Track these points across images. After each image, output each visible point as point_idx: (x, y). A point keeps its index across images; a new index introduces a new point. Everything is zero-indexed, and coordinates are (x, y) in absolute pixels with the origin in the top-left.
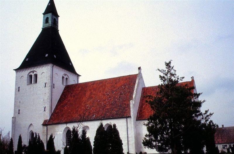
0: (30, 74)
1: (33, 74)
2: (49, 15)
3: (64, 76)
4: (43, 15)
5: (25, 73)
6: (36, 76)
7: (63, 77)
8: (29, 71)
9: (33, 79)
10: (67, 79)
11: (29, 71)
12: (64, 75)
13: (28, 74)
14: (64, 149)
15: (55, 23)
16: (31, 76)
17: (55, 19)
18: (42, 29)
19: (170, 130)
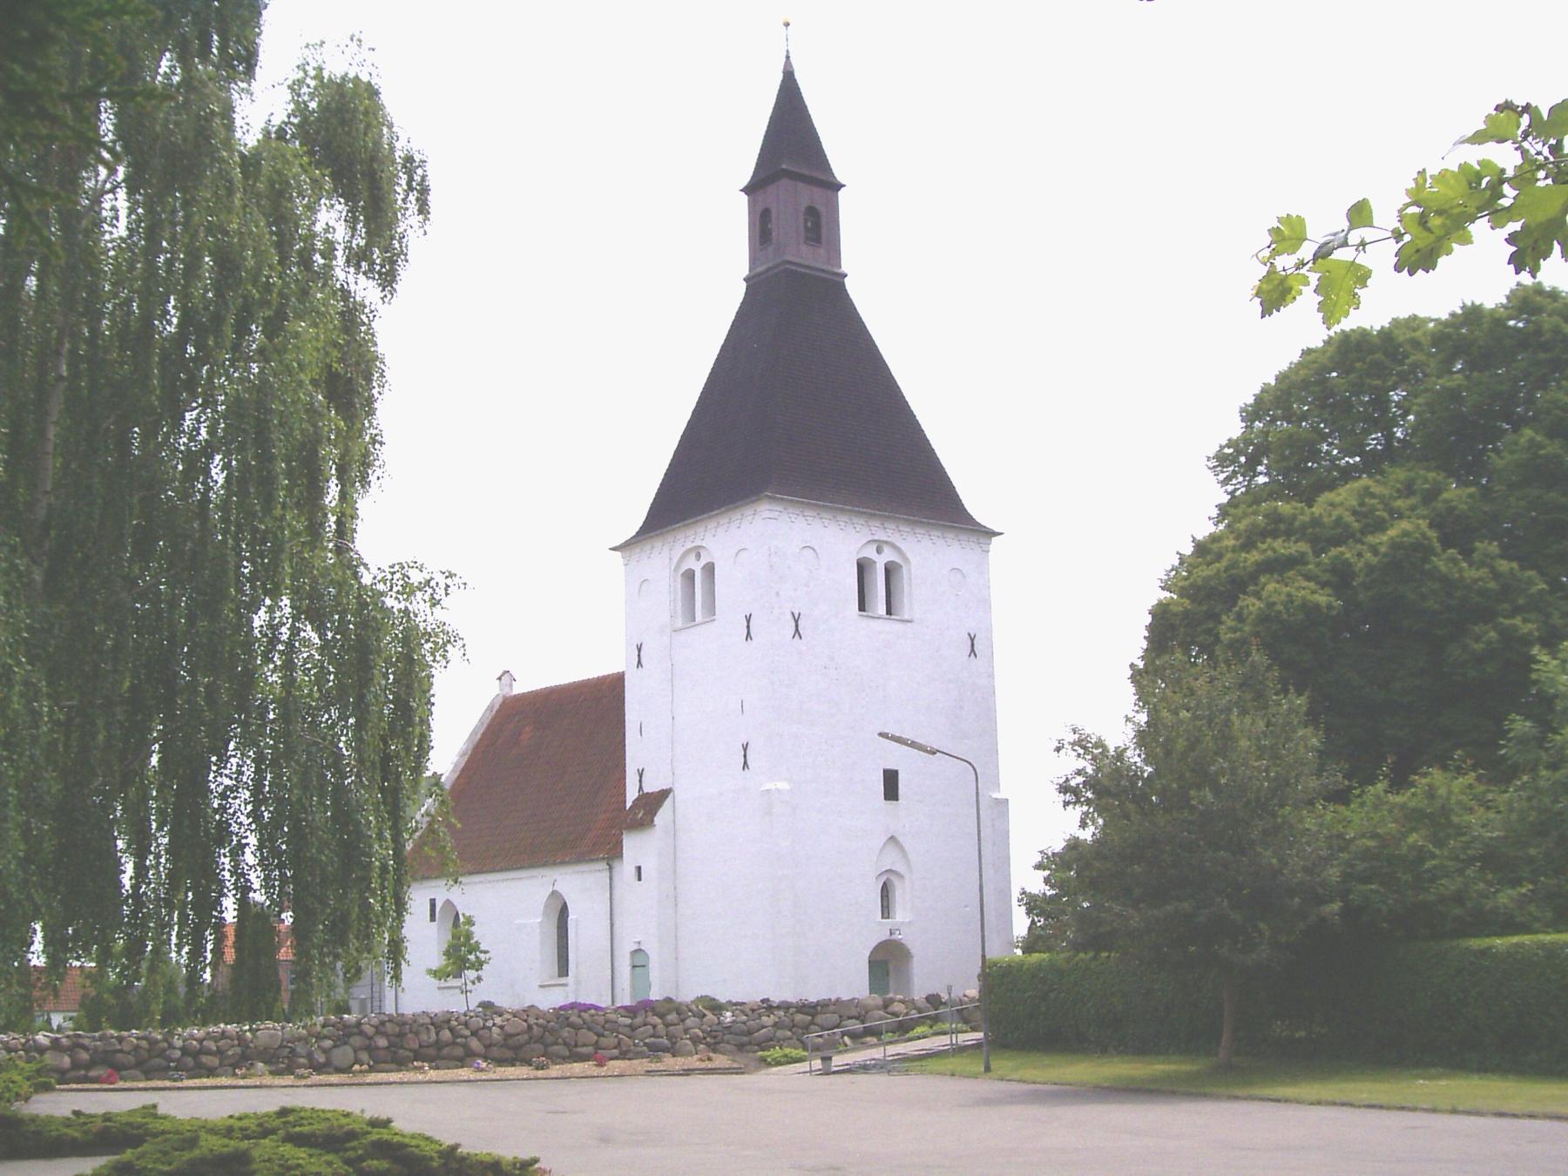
0: (684, 567)
1: (697, 567)
2: (791, 198)
3: (870, 553)
4: (745, 198)
5: (663, 559)
6: (710, 569)
7: (863, 568)
8: (679, 551)
9: (697, 589)
10: (890, 571)
11: (679, 551)
12: (874, 547)
13: (676, 570)
14: (1302, 329)
15: (820, 226)
16: (689, 576)
17: (812, 212)
18: (744, 285)
19: (38, 927)
